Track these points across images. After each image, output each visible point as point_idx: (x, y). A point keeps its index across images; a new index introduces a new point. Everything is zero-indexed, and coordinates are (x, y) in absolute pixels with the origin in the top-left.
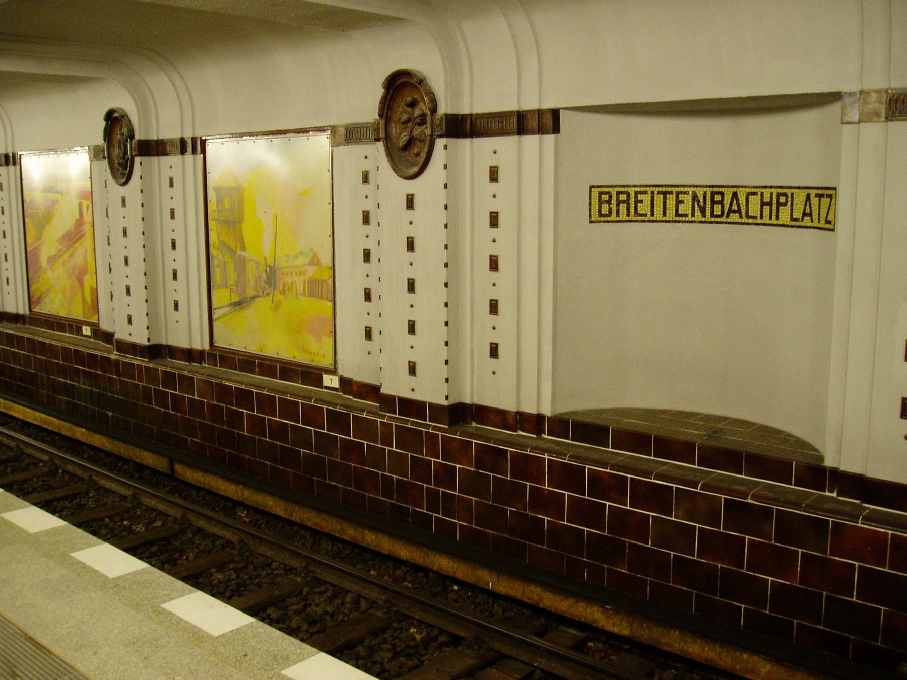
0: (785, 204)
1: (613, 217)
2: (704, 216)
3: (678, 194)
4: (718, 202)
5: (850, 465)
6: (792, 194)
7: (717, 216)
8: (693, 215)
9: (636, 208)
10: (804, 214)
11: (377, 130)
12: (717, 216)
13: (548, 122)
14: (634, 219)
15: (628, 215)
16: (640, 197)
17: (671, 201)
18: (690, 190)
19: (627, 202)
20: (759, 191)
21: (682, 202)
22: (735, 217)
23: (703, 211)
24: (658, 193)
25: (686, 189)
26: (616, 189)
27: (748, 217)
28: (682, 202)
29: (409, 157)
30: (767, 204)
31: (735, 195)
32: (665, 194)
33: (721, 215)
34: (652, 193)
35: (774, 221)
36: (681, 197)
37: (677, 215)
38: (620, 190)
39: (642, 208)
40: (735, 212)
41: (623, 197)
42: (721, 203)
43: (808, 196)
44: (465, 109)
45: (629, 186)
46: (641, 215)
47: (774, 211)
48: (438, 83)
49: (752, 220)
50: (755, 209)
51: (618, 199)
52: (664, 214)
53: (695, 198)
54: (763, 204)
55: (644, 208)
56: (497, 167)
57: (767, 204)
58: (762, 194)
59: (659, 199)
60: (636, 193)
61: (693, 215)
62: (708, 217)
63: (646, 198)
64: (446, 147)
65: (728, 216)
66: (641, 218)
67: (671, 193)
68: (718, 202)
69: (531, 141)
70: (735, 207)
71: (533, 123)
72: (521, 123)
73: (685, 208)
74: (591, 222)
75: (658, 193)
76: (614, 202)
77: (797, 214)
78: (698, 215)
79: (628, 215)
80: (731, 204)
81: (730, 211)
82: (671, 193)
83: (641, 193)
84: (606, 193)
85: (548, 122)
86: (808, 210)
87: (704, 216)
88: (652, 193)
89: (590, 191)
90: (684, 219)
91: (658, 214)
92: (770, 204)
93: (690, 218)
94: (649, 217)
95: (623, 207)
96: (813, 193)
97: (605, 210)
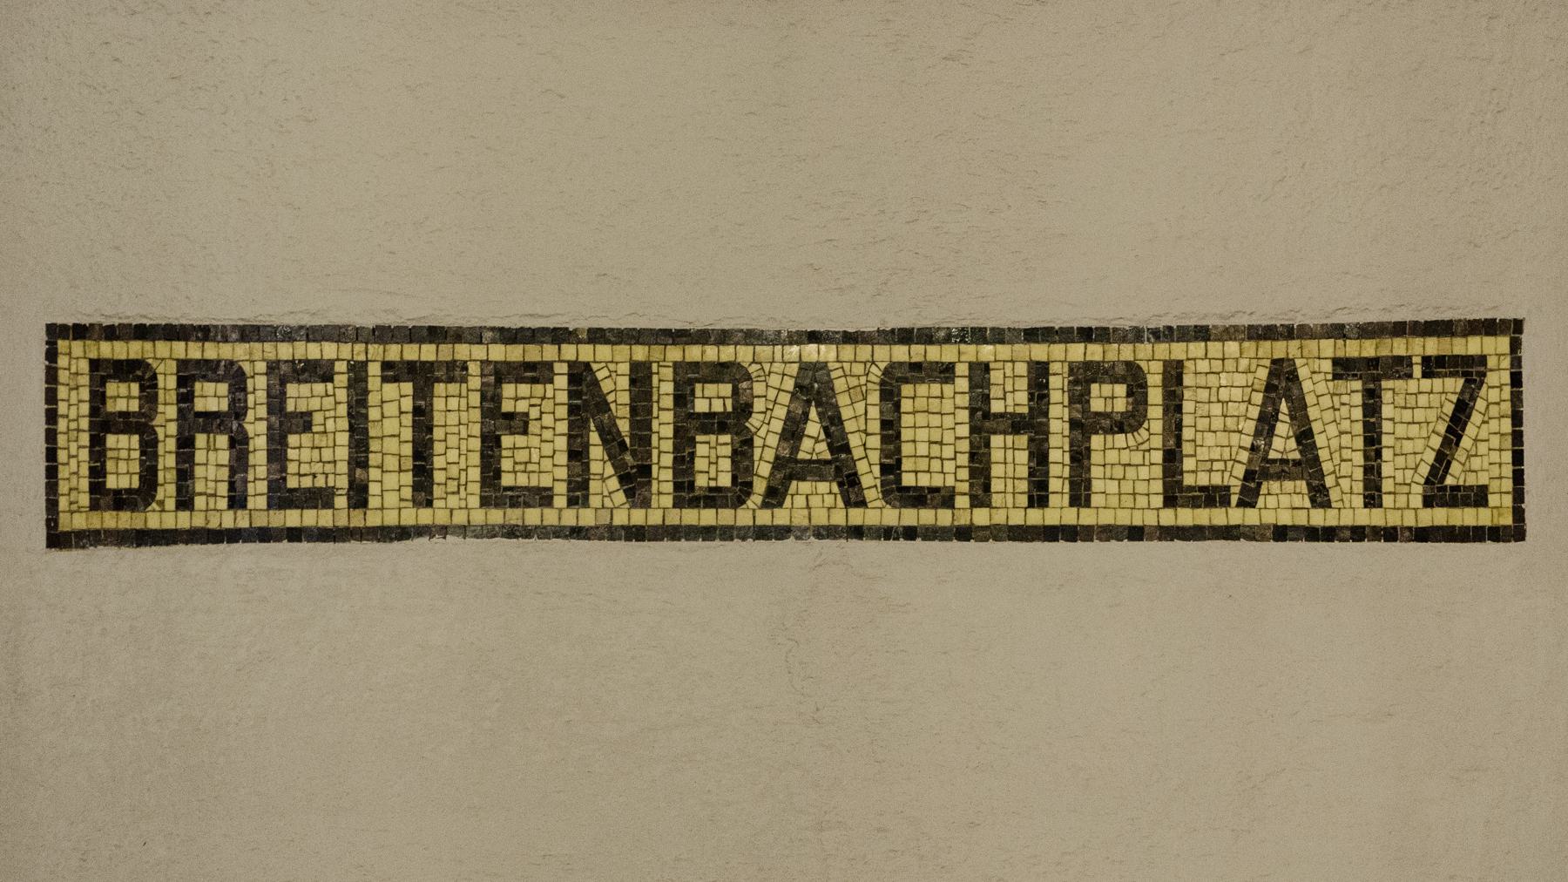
0: (1128, 423)
3: (501, 373)
7: (714, 498)
9: (277, 454)
12: (714, 498)
14: (674, 517)
16: (300, 396)
19: (230, 421)
20: (962, 355)
23: (635, 482)
25: (934, 353)
26: (179, 349)
28: (518, 424)
30: (1016, 424)
32: (422, 377)
33: (739, 492)
34: (358, 372)
35: (1058, 512)
36: (514, 396)
38: (194, 351)
40: (1283, 470)
42: (734, 422)
43: (1282, 380)
46: (918, 497)
47: (1059, 456)
54: (983, 421)
55: (318, 458)
57: (1016, 424)
58: (980, 371)
59: (391, 405)
62: (662, 507)
65: (775, 496)
68: (714, 423)
70: (813, 446)
73: (538, 456)
79: (1039, 497)
80: (793, 432)
81: (790, 469)
84: (720, 372)
88: (358, 372)
89: (52, 355)
90: (310, 518)
91: (390, 493)
92: (1031, 425)
93: (560, 513)
95: (212, 456)
96: (1314, 366)
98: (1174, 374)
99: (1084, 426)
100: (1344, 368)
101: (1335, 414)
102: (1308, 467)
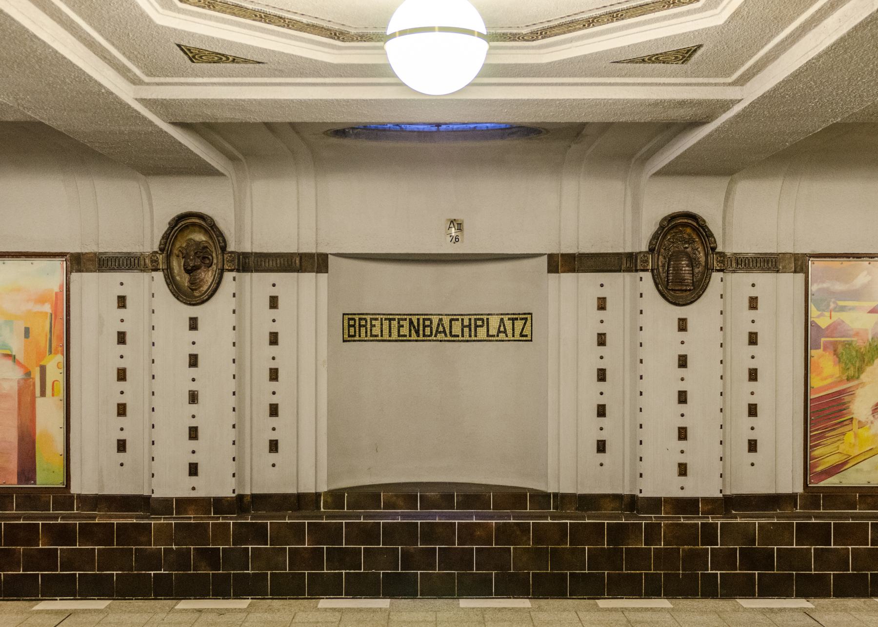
0: (481, 326)
1: (357, 338)
2: (418, 336)
4: (428, 326)
5: (567, 488)
6: (488, 319)
8: (410, 336)
10: (499, 332)
11: (154, 261)
13: (316, 263)
15: (470, 336)
16: (374, 322)
17: (395, 324)
18: (408, 317)
19: (365, 326)
21: (403, 326)
22: (441, 336)
23: (417, 332)
24: (386, 319)
27: (372, 335)
28: (403, 326)
29: (681, 288)
31: (441, 320)
32: (390, 320)
35: (473, 338)
37: (399, 335)
39: (376, 331)
40: (440, 332)
41: (363, 323)
42: (430, 326)
43: (502, 320)
44: (247, 248)
45: (367, 314)
48: (226, 223)
49: (454, 338)
50: (457, 328)
51: (475, 324)
52: (390, 336)
53: (411, 322)
54: (463, 326)
55: (376, 331)
56: (277, 297)
59: (386, 324)
60: (371, 319)
61: (410, 336)
63: (377, 323)
64: (234, 279)
65: (435, 336)
66: (374, 338)
67: (458, 320)
68: (428, 326)
69: (308, 278)
70: (441, 329)
71: (251, 261)
72: (768, 263)
73: (405, 331)
74: (344, 341)
75: (386, 319)
76: (369, 326)
77: (493, 331)
78: (414, 336)
80: (438, 328)
82: (394, 319)
83: (402, 320)
85: (316, 263)
86: (502, 329)
87: (418, 336)
92: (469, 326)
94: (380, 338)
95: (363, 330)
96: (506, 318)
97: (352, 333)
98: (488, 319)
99: (476, 326)
100: (509, 319)
101: (508, 324)
102: (505, 332)
